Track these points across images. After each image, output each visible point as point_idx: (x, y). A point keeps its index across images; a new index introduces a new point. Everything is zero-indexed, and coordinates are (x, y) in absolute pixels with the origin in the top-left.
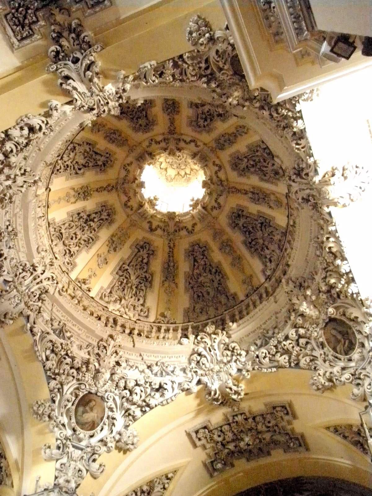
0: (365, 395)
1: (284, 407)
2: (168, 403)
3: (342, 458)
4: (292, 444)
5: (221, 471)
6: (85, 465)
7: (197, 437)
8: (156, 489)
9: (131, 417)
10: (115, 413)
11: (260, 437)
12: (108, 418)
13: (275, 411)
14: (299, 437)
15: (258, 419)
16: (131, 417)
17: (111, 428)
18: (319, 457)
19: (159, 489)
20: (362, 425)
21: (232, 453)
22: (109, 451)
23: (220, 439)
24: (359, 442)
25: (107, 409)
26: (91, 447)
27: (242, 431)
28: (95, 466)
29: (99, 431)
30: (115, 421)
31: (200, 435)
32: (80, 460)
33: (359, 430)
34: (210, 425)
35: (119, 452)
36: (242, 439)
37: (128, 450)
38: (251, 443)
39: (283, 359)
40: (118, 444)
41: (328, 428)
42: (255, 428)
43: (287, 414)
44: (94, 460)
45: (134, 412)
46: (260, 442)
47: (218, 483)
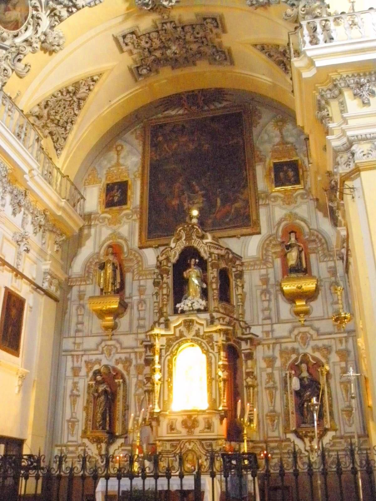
0: (297, 16)
1: (214, 19)
2: (96, 5)
3: (264, 75)
4: (218, 57)
5: (146, 76)
6: (10, 65)
7: (124, 42)
8: (82, 90)
9: (56, 18)
10: (40, 12)
11: (187, 46)
12: (33, 17)
13: (205, 23)
14: (226, 51)
15: (187, 29)
16: (56, 18)
17: (36, 28)
18: (243, 72)
19: (84, 90)
20: (288, 44)
21: (157, 61)
22: (34, 52)
23: (147, 46)
24: (283, 62)
25: (30, 8)
26: (16, 47)
27: (169, 40)
28: (20, 66)
29: (23, 31)
30: (40, 21)
31: (128, 40)
32: (5, 60)
33: (285, 51)
34: (138, 31)
35: (45, 52)
36: (169, 48)
37: (54, 51)
38: (178, 52)
40: (43, 45)
41: (255, 45)
42: (183, 38)
43: (217, 27)
44: (19, 60)
45: (60, 12)
46: (187, 52)
47: (142, 88)
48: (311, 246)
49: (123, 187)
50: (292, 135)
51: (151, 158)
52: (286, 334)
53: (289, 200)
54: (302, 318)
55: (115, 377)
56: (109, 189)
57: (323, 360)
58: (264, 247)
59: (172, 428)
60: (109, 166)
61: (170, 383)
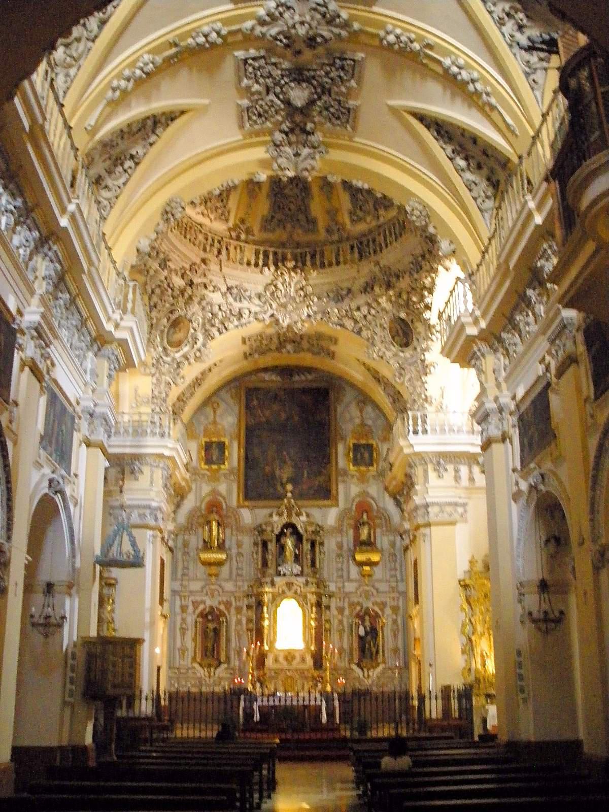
39: (349, 324)
48: (377, 521)
49: (222, 446)
50: (370, 418)
51: (247, 423)
52: (353, 590)
53: (363, 479)
54: (366, 580)
55: (221, 616)
56: (208, 447)
57: (380, 613)
58: (341, 518)
59: (276, 660)
60: (206, 422)
61: (274, 629)
